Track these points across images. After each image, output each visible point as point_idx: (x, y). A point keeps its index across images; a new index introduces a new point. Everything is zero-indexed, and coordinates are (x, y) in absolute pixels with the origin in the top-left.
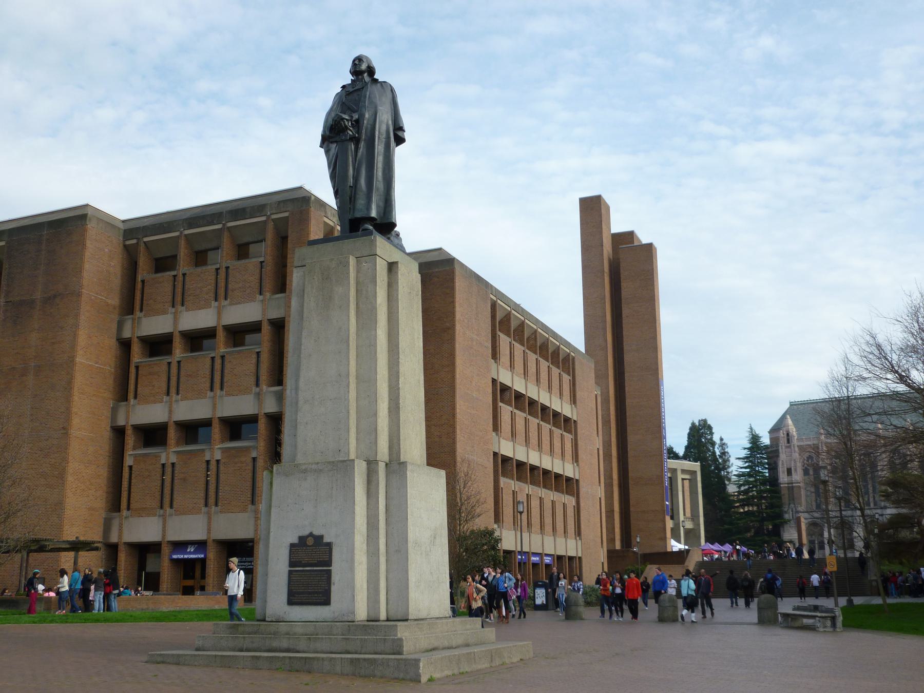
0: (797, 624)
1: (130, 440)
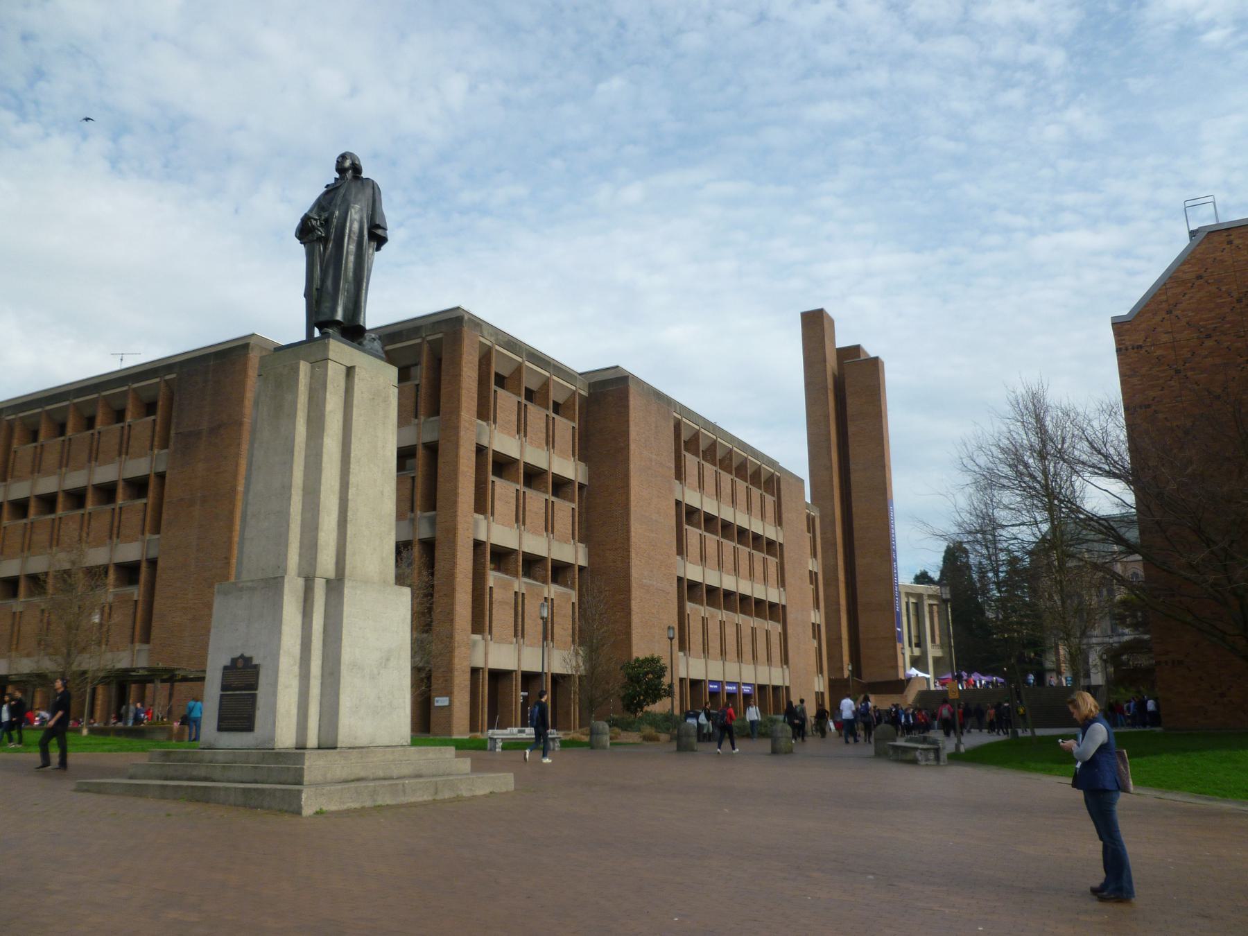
0: (909, 756)
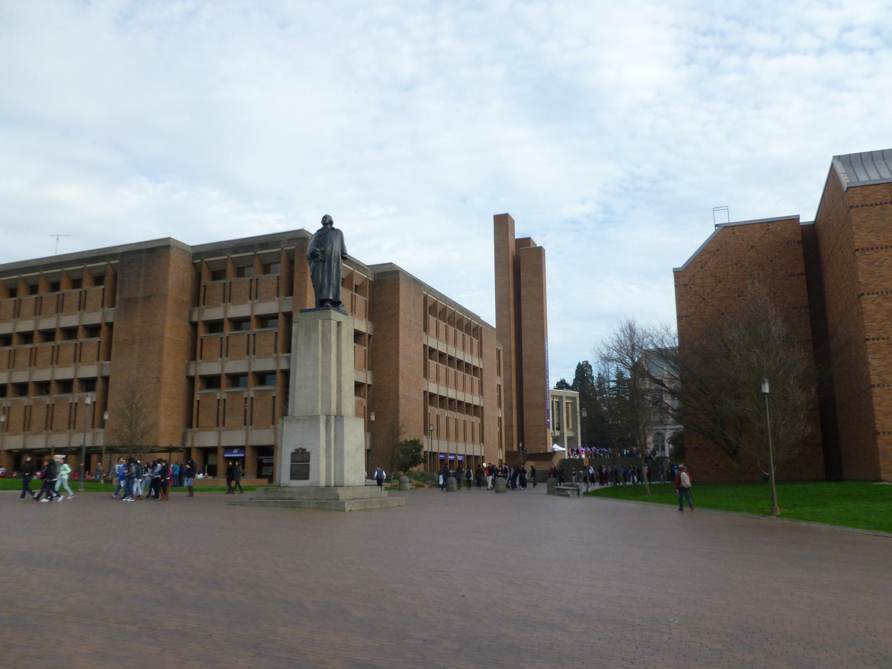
1: (198, 384)
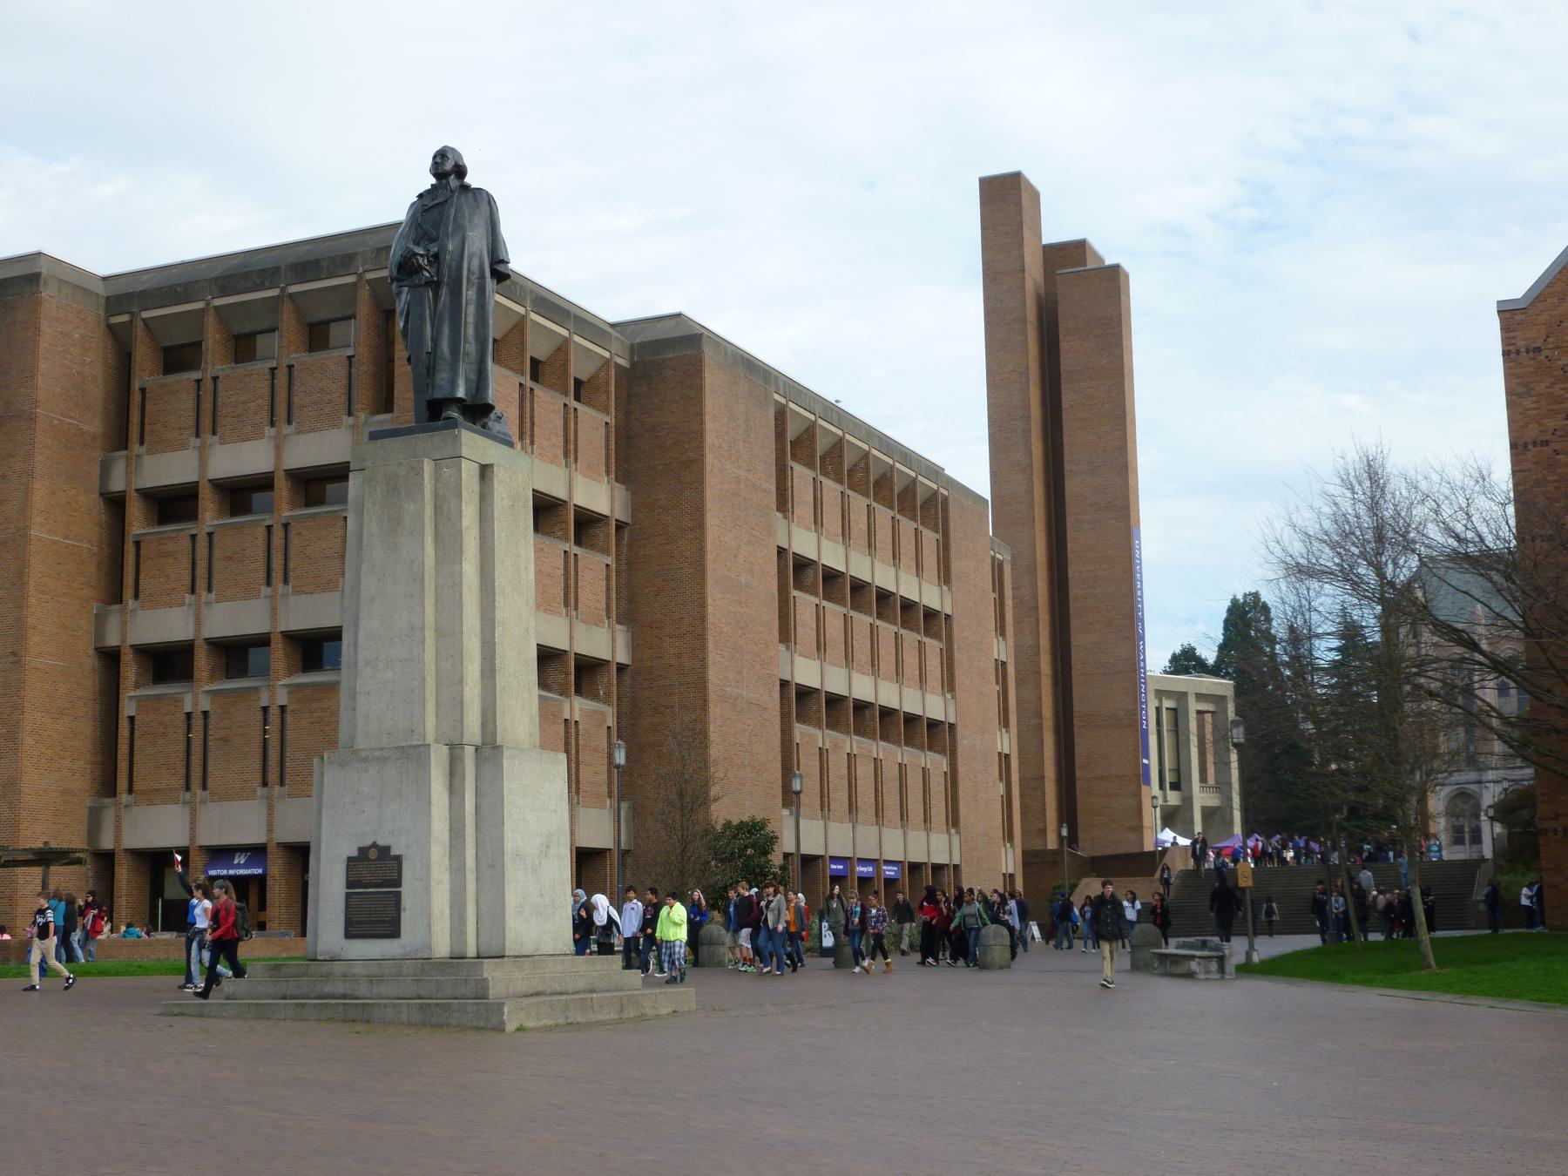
0: (1181, 969)
1: (130, 670)
